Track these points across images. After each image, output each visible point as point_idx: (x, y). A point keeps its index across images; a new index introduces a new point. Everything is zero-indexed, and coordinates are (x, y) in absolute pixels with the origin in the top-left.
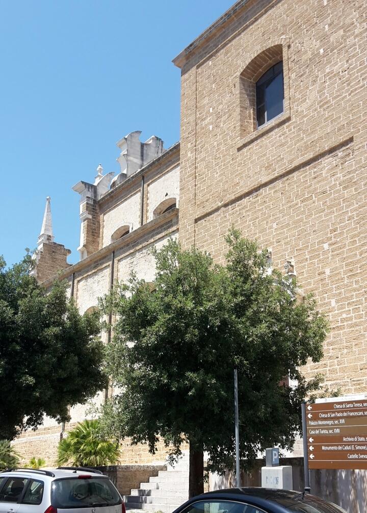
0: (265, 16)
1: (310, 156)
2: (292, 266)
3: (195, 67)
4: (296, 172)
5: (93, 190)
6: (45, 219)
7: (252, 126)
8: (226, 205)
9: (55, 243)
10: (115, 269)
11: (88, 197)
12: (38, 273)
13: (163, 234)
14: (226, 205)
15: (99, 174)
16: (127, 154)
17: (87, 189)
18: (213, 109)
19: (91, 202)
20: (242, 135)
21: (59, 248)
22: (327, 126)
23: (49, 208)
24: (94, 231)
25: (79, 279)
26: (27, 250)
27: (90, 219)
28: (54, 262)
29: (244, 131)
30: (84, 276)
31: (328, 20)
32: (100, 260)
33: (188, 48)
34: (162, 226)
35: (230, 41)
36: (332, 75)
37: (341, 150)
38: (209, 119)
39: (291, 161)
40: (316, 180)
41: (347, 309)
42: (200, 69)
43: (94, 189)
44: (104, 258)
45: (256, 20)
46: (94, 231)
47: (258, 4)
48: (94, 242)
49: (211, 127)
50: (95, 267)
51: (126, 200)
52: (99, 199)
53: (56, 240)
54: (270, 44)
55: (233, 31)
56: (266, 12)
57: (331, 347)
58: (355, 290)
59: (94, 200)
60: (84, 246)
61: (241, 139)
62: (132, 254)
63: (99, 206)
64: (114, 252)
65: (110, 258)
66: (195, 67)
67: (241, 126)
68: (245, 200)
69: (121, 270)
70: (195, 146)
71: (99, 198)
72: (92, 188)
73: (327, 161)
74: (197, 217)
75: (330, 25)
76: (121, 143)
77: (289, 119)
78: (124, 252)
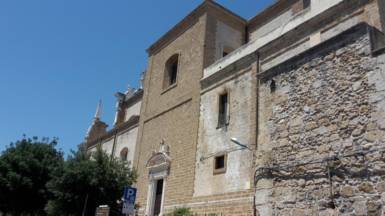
0: (176, 40)
1: (180, 103)
2: (169, 148)
3: (153, 55)
4: (176, 108)
5: (123, 96)
6: (97, 110)
7: (168, 85)
8: (154, 118)
9: (101, 122)
10: (116, 139)
11: (120, 100)
12: (90, 136)
13: (134, 126)
14: (154, 118)
15: (128, 89)
16: (143, 80)
17: (120, 96)
18: (156, 75)
19: (122, 102)
20: (163, 89)
21: (102, 124)
22: (186, 91)
23: (100, 105)
24: (122, 115)
25: (103, 141)
26: (54, 138)
27: (120, 110)
28: (99, 131)
29: (164, 86)
30: (106, 140)
31: (192, 48)
32: (112, 134)
33: (151, 46)
34: (134, 122)
35: (165, 47)
36: (191, 71)
37: (189, 102)
38: (154, 78)
39: (175, 103)
40: (180, 113)
41: (182, 169)
42: (155, 56)
43: (124, 96)
44: (113, 133)
45: (173, 41)
46: (122, 115)
47: (174, 34)
48: (121, 121)
49: (155, 82)
50: (110, 137)
51: (136, 103)
52: (126, 101)
53: (102, 120)
54: (176, 52)
55: (166, 43)
56: (177, 38)
57: (175, 184)
58: (185, 161)
59: (123, 101)
60: (116, 123)
61: (162, 90)
62: (123, 133)
63: (125, 104)
64: (116, 131)
65: (115, 134)
66: (153, 55)
67: (163, 84)
68: (160, 117)
69: (118, 140)
70: (149, 89)
71: (126, 100)
72: (123, 95)
73: (185, 106)
74: (145, 121)
75: (193, 50)
76: (141, 74)
77: (176, 86)
78: (120, 132)
